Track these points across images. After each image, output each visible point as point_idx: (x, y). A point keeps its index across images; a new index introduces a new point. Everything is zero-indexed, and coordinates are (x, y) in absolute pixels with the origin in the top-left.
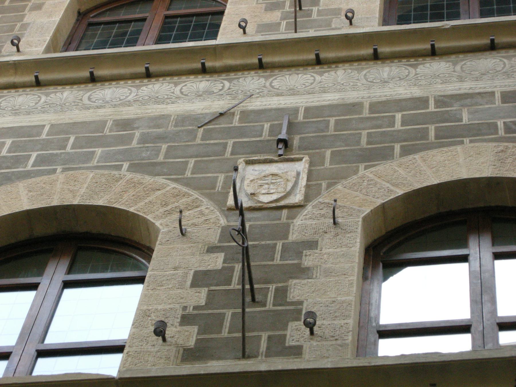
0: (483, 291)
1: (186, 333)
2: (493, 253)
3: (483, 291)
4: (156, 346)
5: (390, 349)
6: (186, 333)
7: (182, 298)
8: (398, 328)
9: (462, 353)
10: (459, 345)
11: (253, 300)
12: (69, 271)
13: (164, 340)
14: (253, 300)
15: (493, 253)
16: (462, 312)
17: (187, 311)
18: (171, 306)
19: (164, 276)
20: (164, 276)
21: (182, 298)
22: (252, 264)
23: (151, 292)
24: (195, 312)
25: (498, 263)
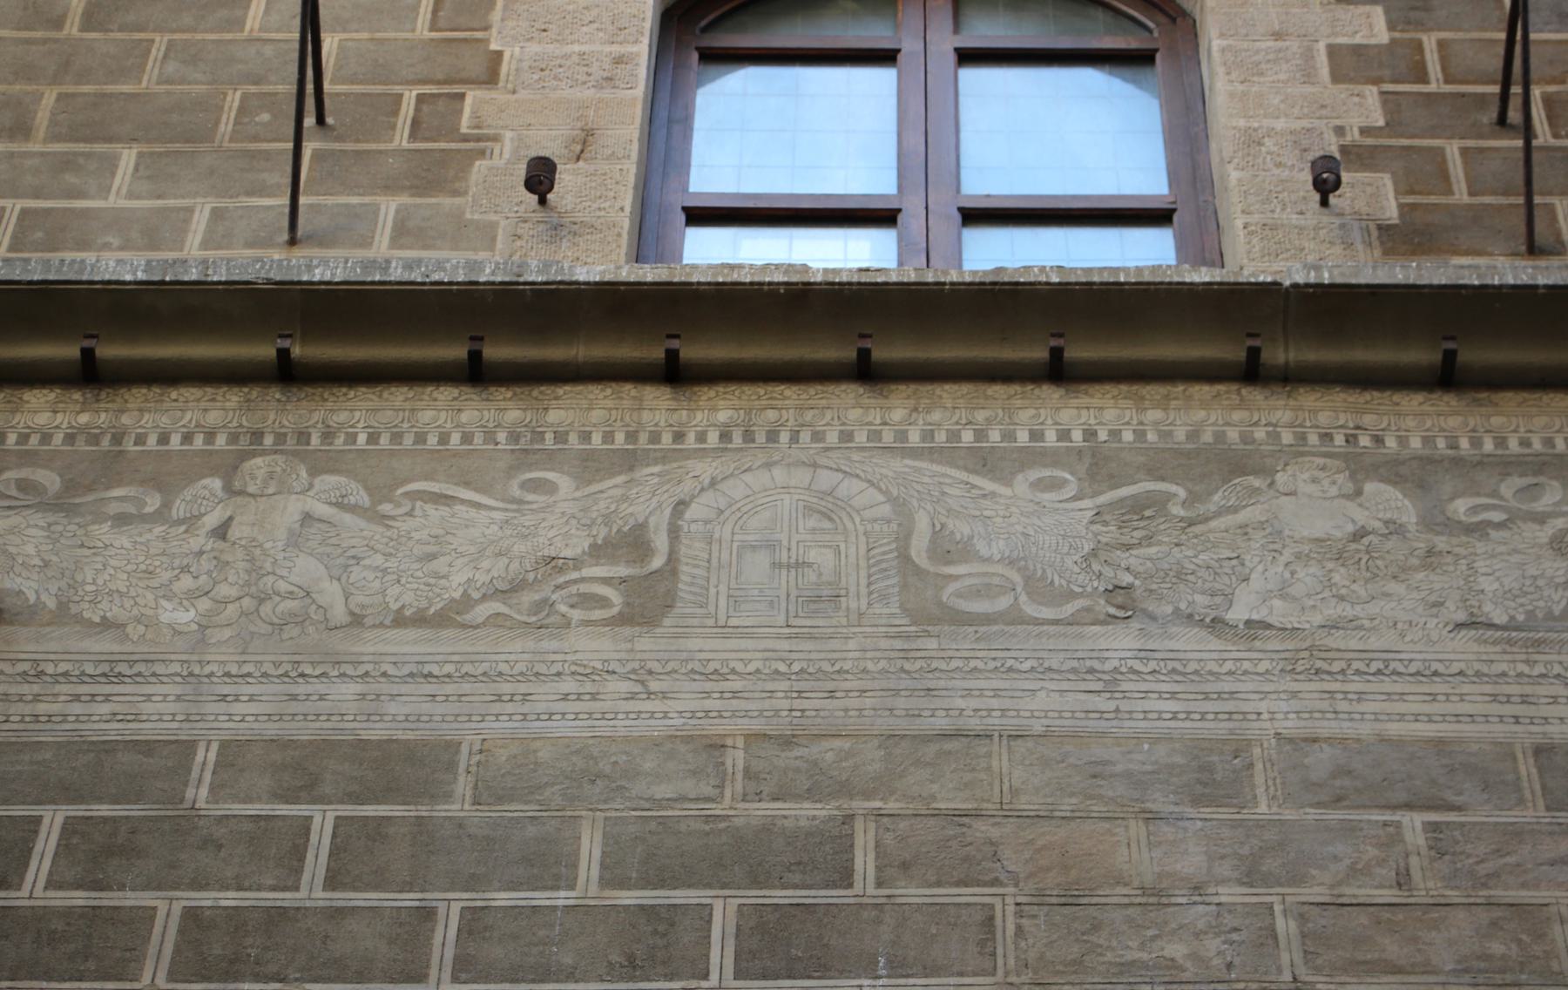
0: (927, 138)
1: (1369, 190)
2: (956, 50)
3: (927, 138)
4: (1308, 215)
5: (710, 252)
6: (1369, 190)
7: (1323, 107)
8: (750, 204)
9: (1155, 269)
10: (1142, 253)
11: (321, 120)
12: (957, 29)
13: (543, 201)
14: (321, 120)
15: (956, 50)
16: (871, 179)
17: (1349, 138)
18: (1305, 123)
19: (1257, 52)
20: (1257, 52)
21: (1323, 107)
22: (1533, 36)
23: (1240, 88)
24: (1370, 141)
25: (974, 78)
